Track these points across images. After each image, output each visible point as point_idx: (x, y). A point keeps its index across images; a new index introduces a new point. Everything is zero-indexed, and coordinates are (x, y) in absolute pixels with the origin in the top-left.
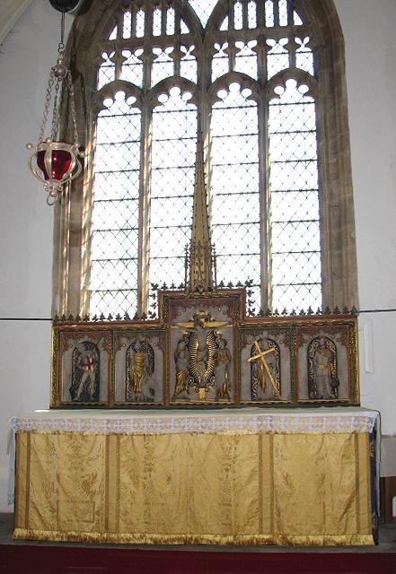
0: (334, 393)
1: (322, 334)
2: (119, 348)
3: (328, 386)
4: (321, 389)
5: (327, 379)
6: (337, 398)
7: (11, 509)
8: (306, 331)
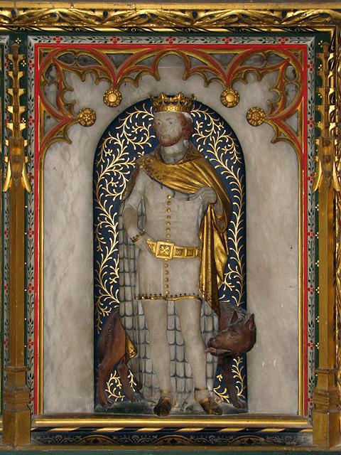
0: (227, 383)
1: (171, 80)
2: (60, 134)
3: (196, 352)
4: (157, 362)
5: (190, 315)
6: (240, 409)
7: (250, 412)
8: (86, 64)
